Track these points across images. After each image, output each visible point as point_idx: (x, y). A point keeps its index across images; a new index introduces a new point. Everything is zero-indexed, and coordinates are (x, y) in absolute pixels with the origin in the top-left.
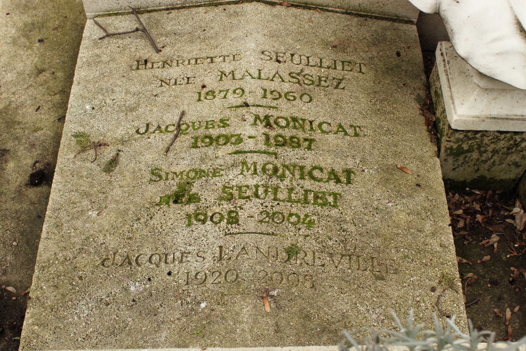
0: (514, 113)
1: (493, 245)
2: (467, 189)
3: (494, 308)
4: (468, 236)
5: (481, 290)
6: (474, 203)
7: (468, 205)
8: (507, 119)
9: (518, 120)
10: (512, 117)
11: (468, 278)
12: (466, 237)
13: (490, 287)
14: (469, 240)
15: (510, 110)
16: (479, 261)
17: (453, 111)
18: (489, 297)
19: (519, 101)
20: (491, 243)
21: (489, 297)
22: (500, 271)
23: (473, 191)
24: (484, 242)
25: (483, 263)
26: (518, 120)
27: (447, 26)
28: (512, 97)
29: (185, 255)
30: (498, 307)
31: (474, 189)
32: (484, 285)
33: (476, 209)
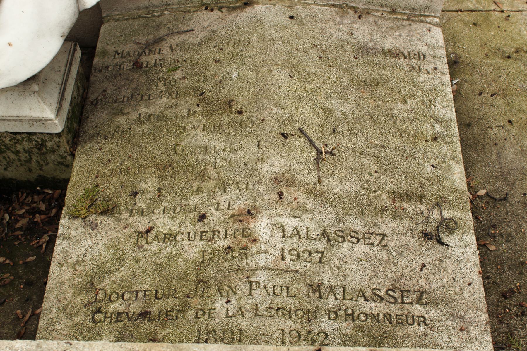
0: (10, 114)
1: (42, 245)
2: (38, 188)
3: (18, 309)
4: (22, 236)
5: (13, 291)
6: (41, 202)
7: (35, 205)
8: (4, 120)
9: (15, 121)
10: (9, 118)
11: (5, 278)
12: (20, 236)
13: (23, 288)
14: (21, 240)
15: (6, 112)
16: (21, 262)
17: (70, 111)
18: (17, 298)
19: (14, 102)
20: (41, 243)
21: (17, 298)
22: (39, 272)
23: (45, 190)
24: (35, 242)
25: (26, 264)
26: (15, 121)
27: (72, 26)
28: (7, 98)
29: (204, 234)
30: (22, 308)
31: (46, 188)
32: (17, 286)
33: (41, 209)
